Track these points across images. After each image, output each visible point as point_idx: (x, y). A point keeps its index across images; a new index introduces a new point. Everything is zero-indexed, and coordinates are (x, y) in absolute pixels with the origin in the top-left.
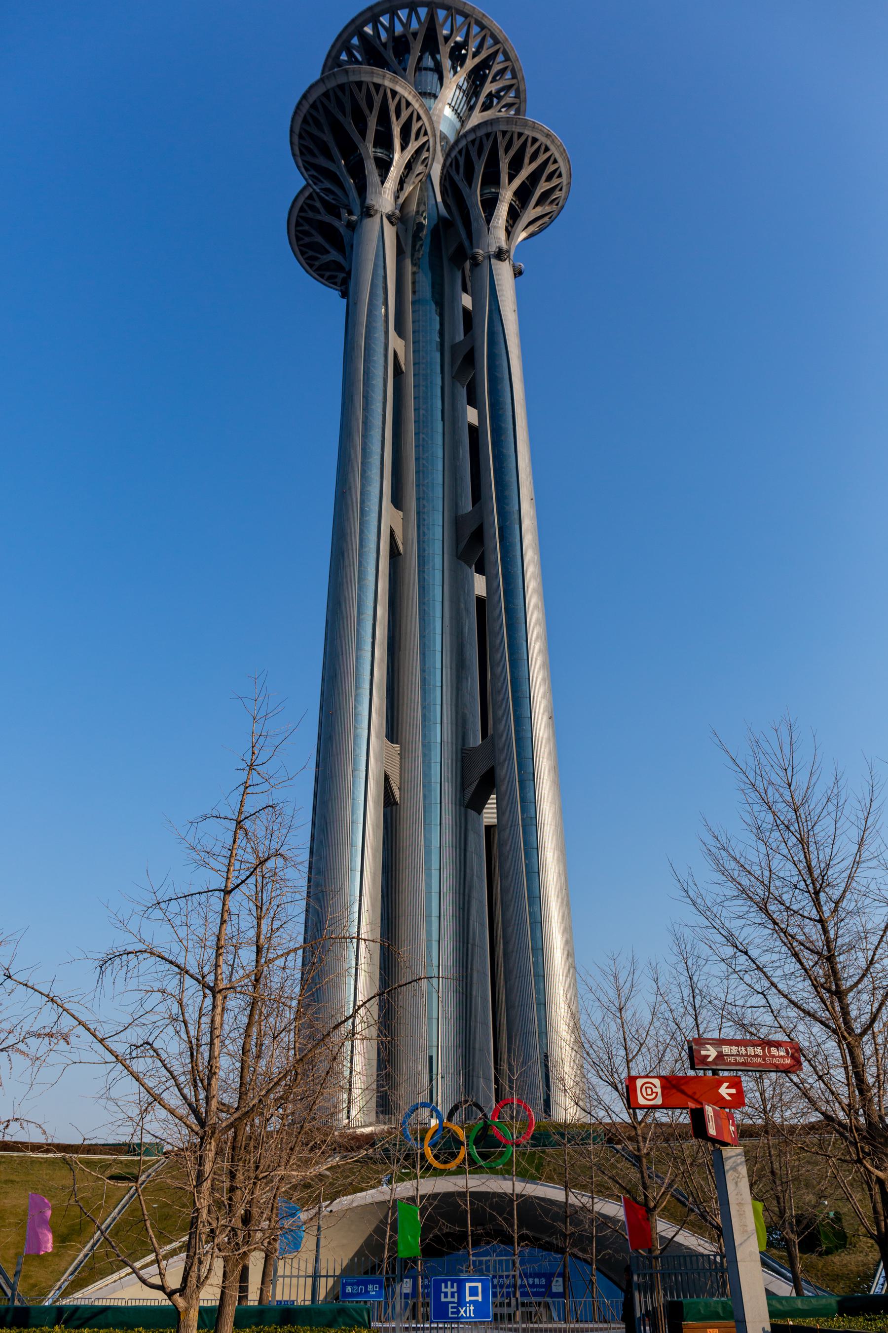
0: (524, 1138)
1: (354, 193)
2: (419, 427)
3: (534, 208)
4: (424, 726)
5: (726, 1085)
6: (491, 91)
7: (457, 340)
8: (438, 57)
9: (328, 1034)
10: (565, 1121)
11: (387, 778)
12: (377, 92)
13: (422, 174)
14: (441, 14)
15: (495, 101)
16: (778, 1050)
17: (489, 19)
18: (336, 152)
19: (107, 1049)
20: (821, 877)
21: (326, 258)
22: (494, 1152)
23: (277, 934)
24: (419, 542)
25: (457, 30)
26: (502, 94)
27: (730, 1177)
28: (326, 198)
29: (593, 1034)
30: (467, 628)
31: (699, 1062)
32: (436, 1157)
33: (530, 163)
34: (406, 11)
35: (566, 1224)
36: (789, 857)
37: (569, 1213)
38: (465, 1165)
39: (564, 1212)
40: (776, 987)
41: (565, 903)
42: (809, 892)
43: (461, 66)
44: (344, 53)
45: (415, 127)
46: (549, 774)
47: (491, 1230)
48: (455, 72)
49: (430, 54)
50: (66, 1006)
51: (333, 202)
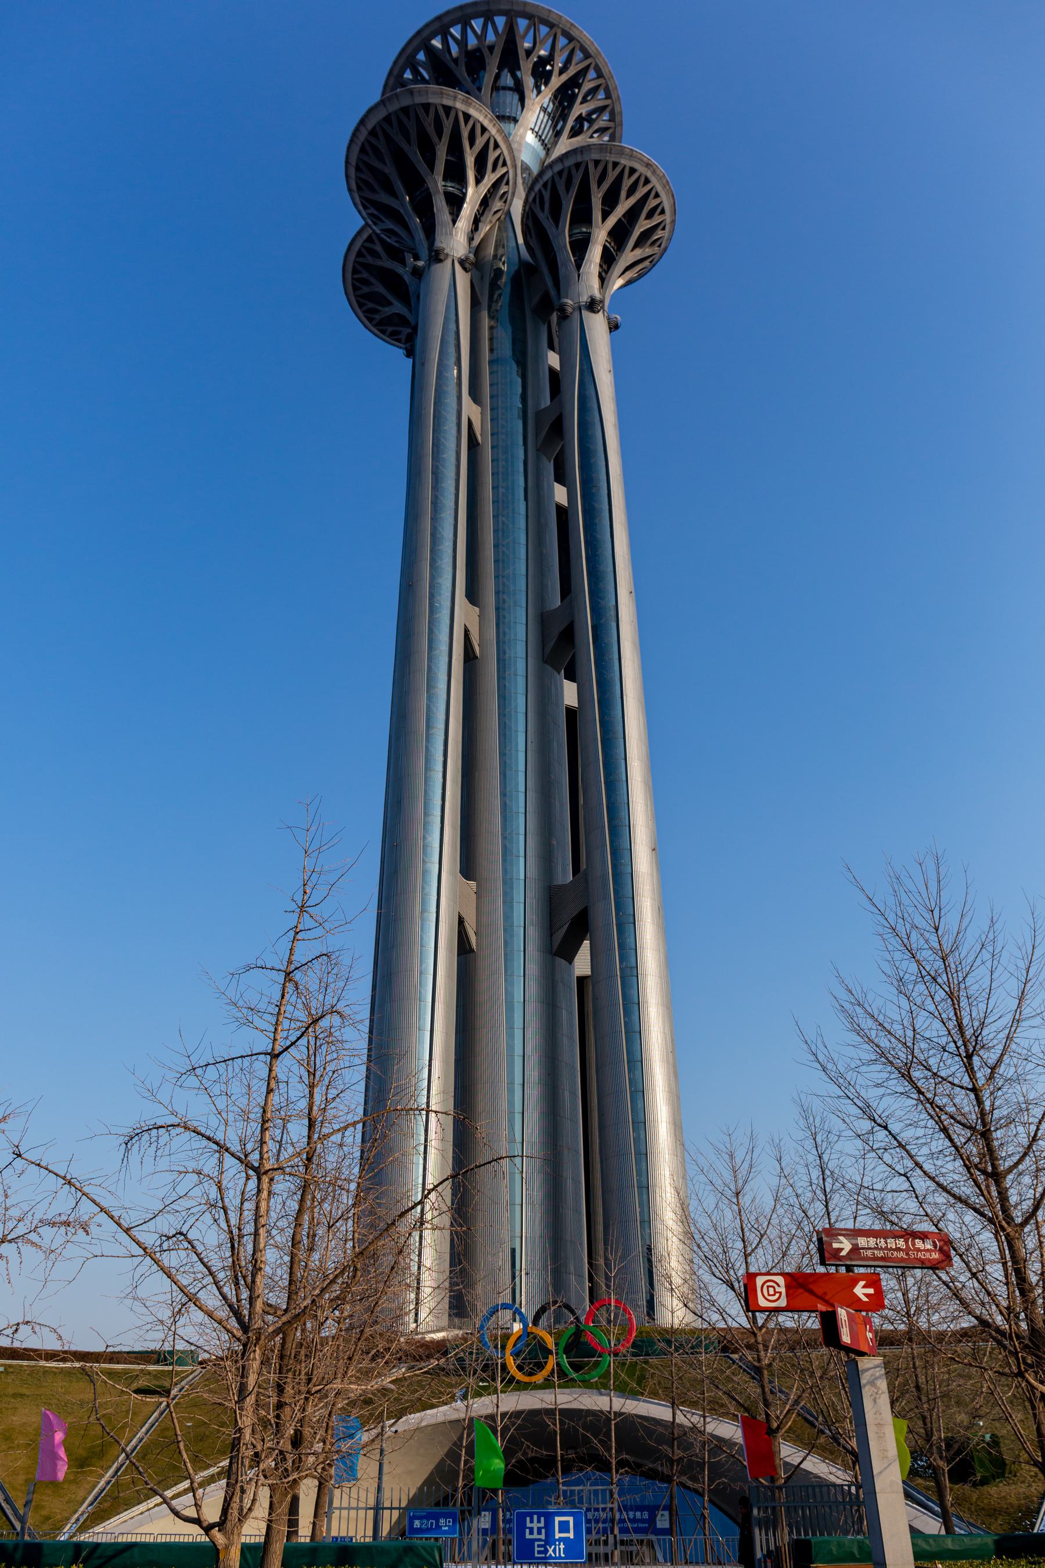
0: (623, 1345)
1: (420, 235)
2: (498, 507)
3: (632, 250)
4: (504, 860)
5: (862, 1283)
6: (581, 114)
7: (543, 406)
8: (518, 73)
9: (393, 1224)
10: (672, 1327)
11: (461, 921)
12: (448, 116)
13: (501, 212)
14: (522, 23)
15: (586, 125)
16: (924, 1243)
17: (578, 29)
18: (399, 186)
19: (134, 1241)
20: (974, 1038)
21: (387, 311)
22: (588, 1363)
23: (332, 1105)
24: (497, 643)
25: (541, 42)
26: (594, 116)
27: (867, 1392)
28: (388, 240)
29: (704, 1223)
30: (555, 744)
31: (830, 1256)
32: (520, 1368)
33: (628, 197)
34: (481, 21)
35: (673, 1448)
36: (936, 1013)
37: (676, 1435)
38: (554, 1377)
39: (671, 1433)
40: (921, 1168)
41: (671, 1067)
42: (960, 1055)
43: (546, 85)
44: (408, 71)
45: (492, 156)
46: (653, 916)
47: (584, 1454)
48: (539, 92)
49: (509, 71)
50: (86, 1189)
51: (397, 245)
